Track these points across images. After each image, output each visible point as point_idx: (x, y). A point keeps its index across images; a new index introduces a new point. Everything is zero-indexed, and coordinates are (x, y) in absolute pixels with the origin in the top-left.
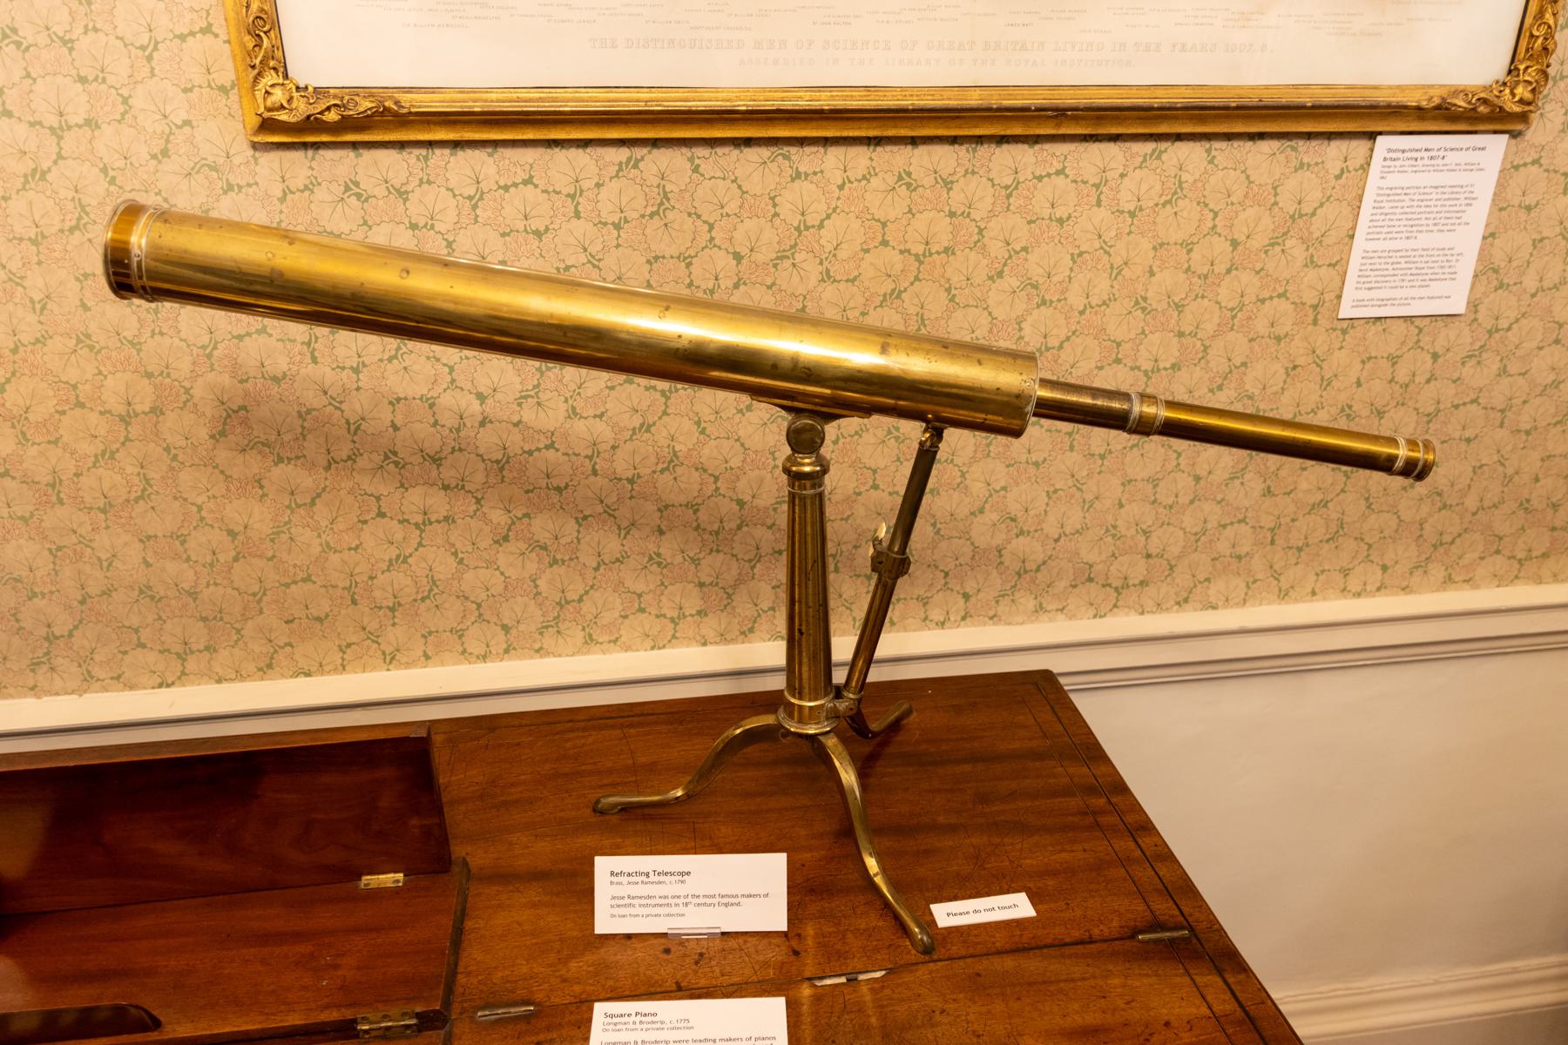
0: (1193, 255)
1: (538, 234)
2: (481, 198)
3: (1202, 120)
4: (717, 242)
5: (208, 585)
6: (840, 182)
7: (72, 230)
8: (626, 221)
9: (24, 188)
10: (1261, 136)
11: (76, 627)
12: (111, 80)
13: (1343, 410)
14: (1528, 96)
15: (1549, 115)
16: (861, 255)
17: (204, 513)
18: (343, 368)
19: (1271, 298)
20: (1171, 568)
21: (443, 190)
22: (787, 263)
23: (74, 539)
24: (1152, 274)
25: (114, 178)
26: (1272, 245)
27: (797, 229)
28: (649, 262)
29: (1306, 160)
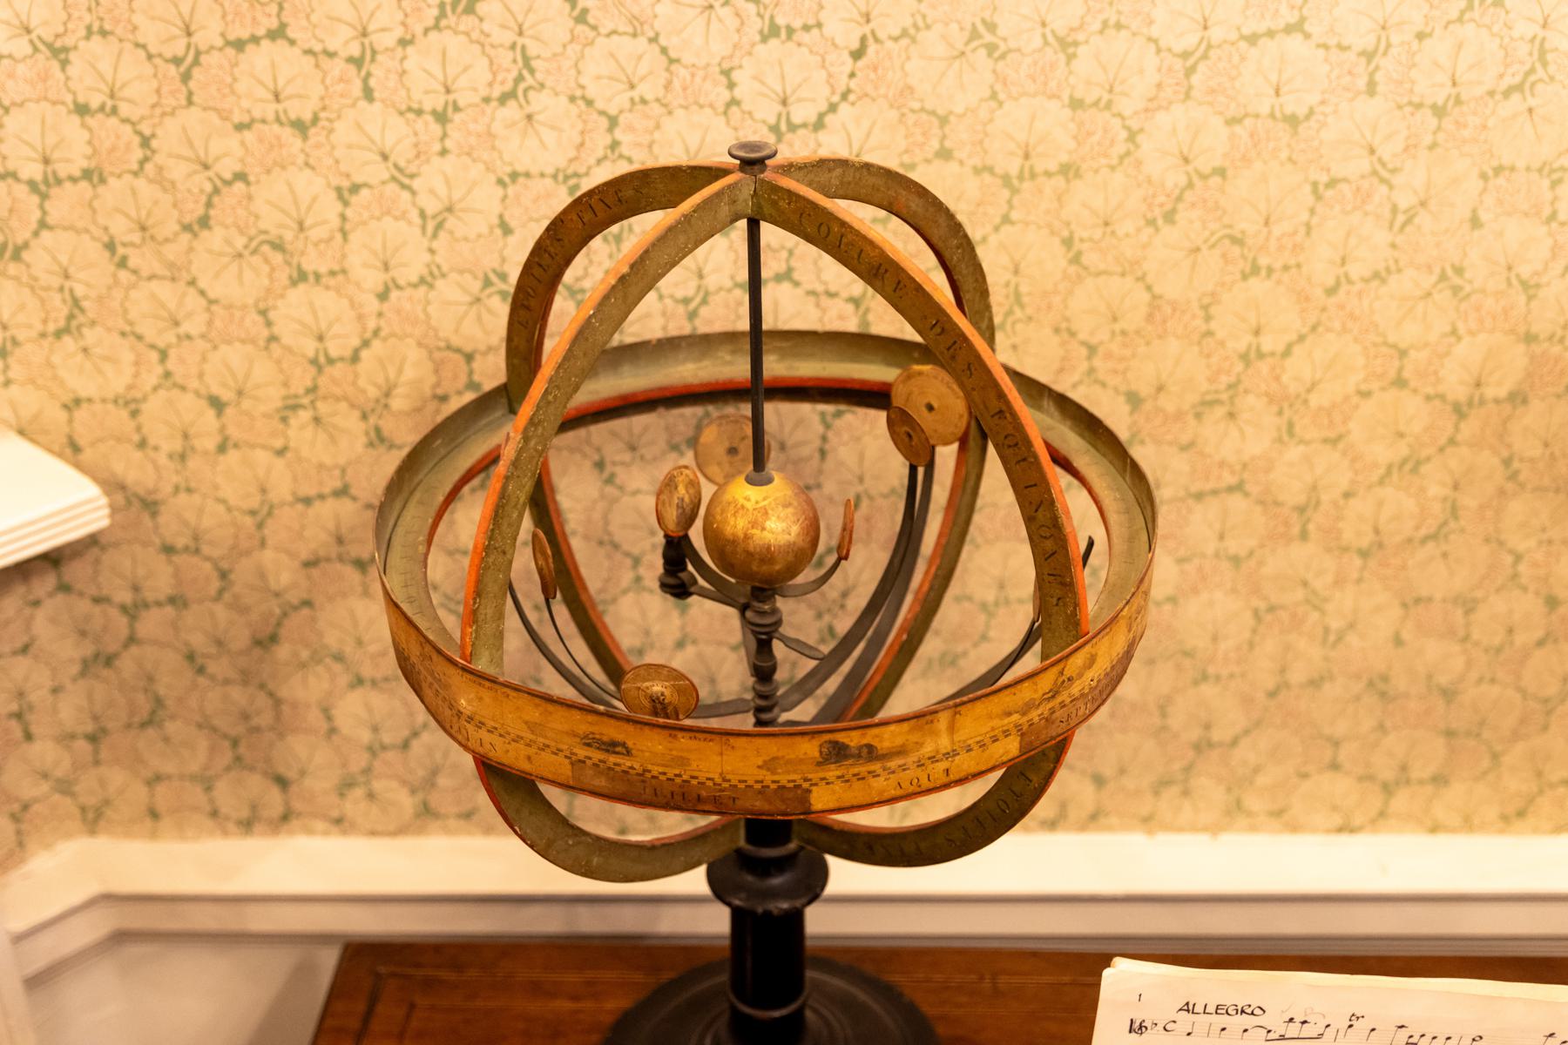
1: (300, 127)
2: (196, 62)
5: (1480, 680)
6: (1331, 282)
8: (457, 108)
9: (437, 27)
11: (1247, 732)
16: (1355, 399)
17: (1522, 568)
18: (1419, 106)
21: (128, 46)
23: (1300, 594)
28: (500, 182)
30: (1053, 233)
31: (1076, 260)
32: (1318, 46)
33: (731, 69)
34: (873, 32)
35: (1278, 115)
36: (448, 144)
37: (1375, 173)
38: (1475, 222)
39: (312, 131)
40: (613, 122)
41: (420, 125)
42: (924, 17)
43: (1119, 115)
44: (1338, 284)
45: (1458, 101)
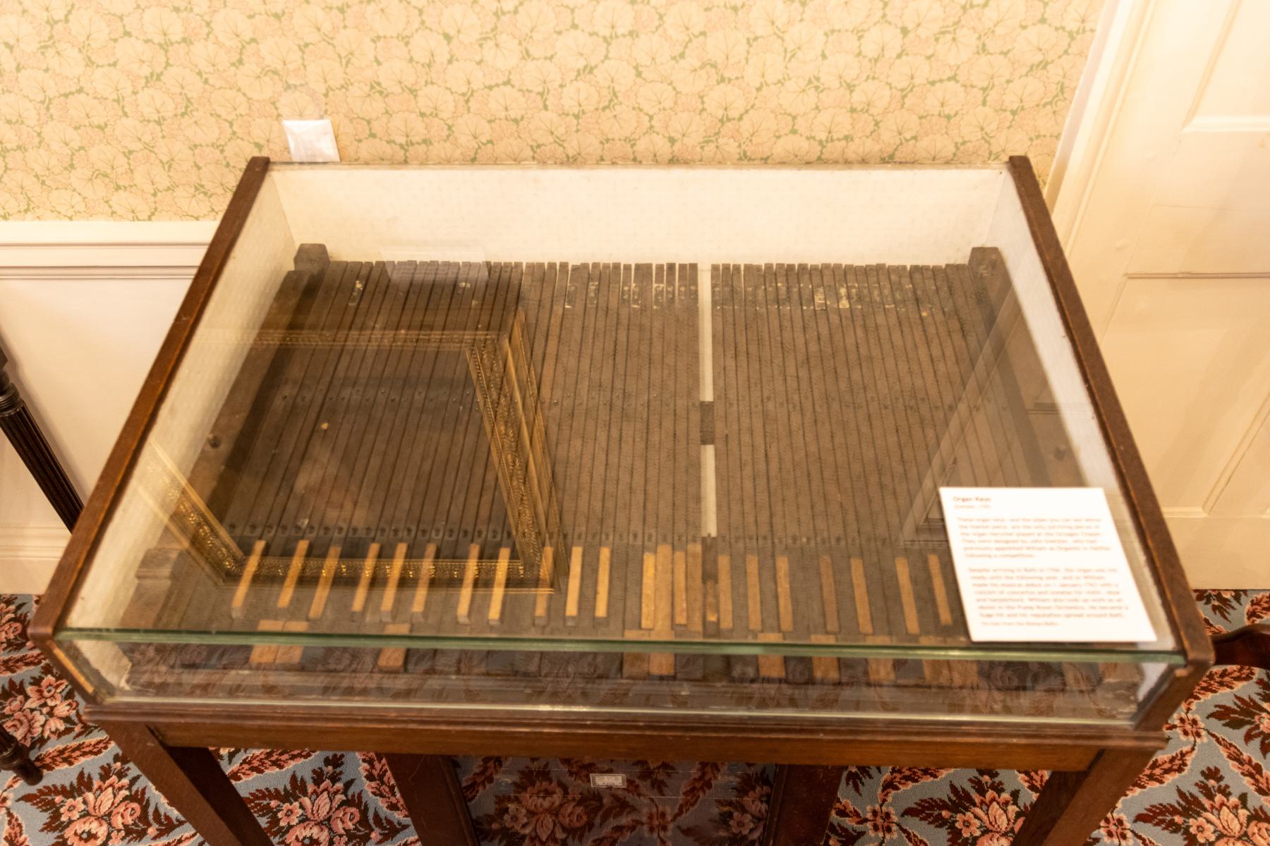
1: (276, 16)
6: (758, 85)
7: (183, 115)
8: (584, 113)
12: (196, 10)
13: (810, 82)
16: (555, 36)
18: (149, 121)
22: (491, 43)
27: (721, 121)
31: (639, 74)
36: (347, 23)
38: (824, 56)
40: (421, 12)
41: (568, 119)
45: (1023, 109)
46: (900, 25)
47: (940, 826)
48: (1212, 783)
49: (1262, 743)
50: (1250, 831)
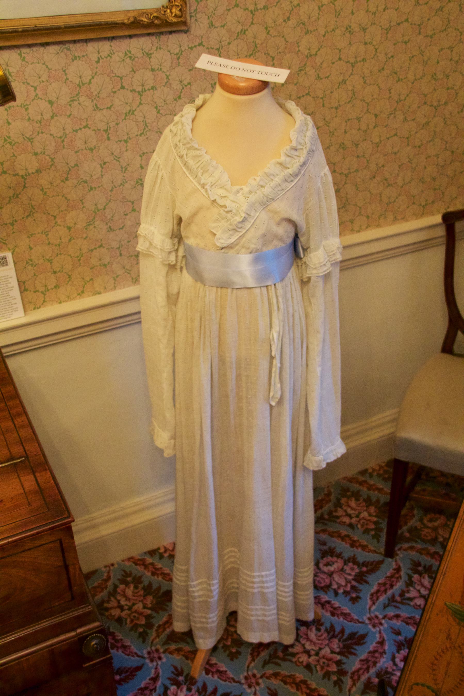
0: (30, 111)
2: (181, 54)
3: (8, 39)
4: (39, 96)
10: (48, 44)
14: (178, 13)
15: (200, 20)
18: (121, 141)
19: (80, 129)
20: (70, 277)
24: (9, 124)
25: (46, 192)
26: (300, 71)
29: (77, 55)
30: (152, 106)
32: (93, 130)
33: (66, 70)
34: (101, 56)
35: (87, 148)
37: (115, 159)
38: (353, 13)
39: (94, 151)
42: (113, 50)
43: (164, 72)
44: (113, 188)
46: (374, 113)
47: (119, 669)
48: (354, 595)
49: (334, 631)
50: (329, 579)
